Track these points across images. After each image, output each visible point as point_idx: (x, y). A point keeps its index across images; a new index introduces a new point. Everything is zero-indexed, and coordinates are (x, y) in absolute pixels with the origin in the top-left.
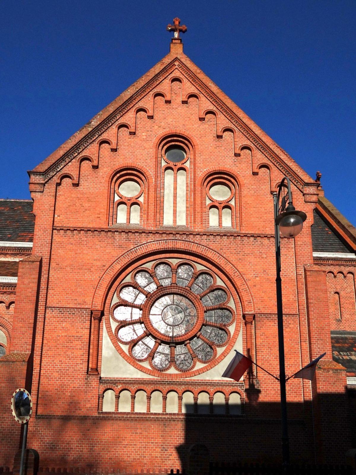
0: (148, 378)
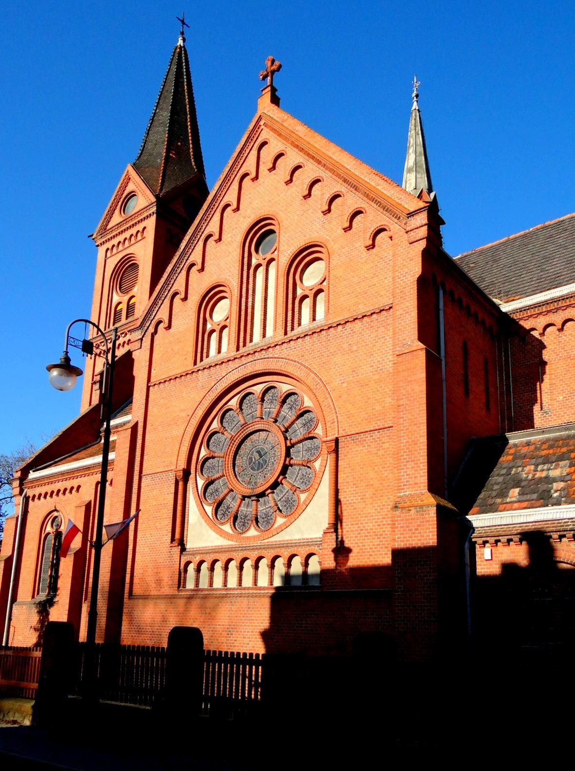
0: (227, 544)
